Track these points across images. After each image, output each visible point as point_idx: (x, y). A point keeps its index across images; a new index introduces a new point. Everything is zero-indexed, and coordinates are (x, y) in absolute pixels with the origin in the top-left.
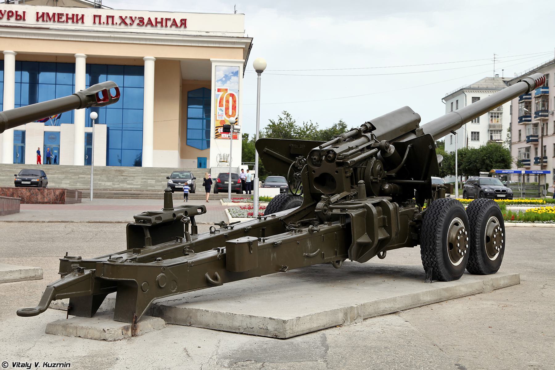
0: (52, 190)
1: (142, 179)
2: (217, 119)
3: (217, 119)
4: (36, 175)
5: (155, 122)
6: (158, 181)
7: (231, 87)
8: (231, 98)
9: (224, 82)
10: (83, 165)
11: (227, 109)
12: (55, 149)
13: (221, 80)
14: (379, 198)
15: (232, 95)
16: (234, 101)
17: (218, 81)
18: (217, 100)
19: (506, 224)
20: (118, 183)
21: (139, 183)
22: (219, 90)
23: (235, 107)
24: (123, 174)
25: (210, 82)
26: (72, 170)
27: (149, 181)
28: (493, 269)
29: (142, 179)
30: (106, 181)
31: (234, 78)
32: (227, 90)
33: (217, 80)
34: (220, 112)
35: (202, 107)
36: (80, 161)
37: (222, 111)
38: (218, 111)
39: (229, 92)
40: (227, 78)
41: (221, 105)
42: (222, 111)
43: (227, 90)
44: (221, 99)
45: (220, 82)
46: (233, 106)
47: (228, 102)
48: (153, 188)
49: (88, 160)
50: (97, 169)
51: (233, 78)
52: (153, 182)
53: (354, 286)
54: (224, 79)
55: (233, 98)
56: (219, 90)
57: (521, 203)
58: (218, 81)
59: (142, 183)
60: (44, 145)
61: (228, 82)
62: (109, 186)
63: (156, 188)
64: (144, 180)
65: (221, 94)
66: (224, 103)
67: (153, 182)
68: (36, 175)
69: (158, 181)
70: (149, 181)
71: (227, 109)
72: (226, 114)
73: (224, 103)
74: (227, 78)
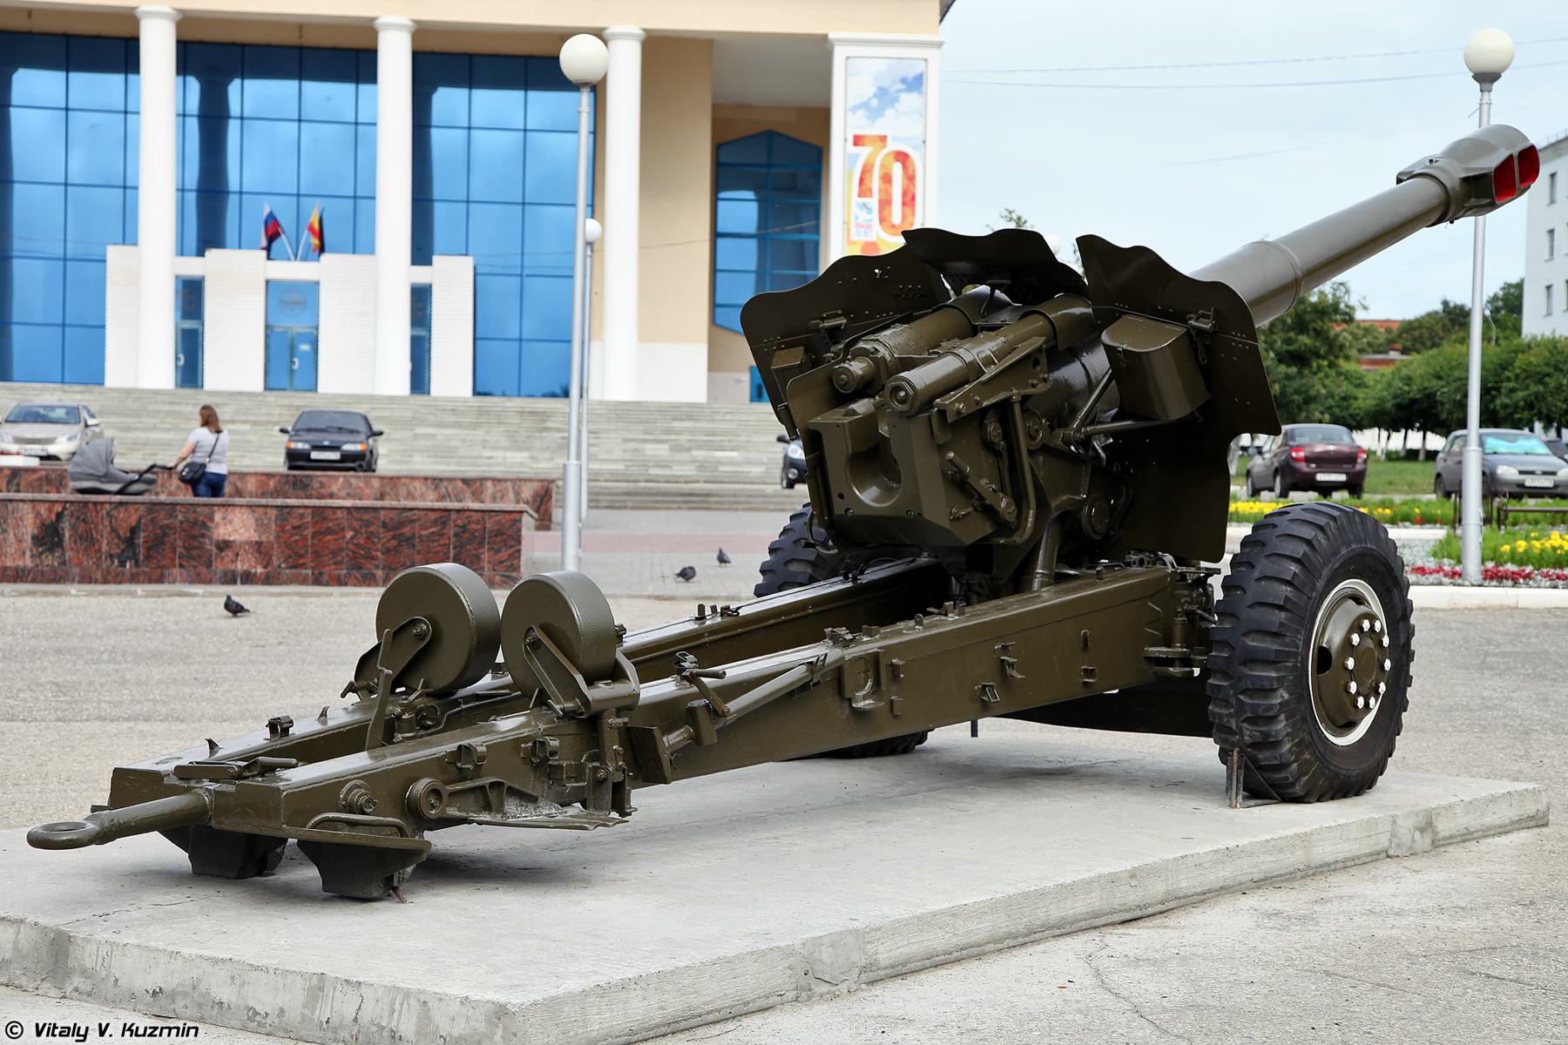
0: (509, 484)
1: (626, 440)
2: (853, 238)
3: (853, 238)
4: (352, 432)
5: (643, 247)
6: (676, 448)
7: (898, 126)
8: (897, 169)
9: (875, 113)
10: (258, 385)
11: (885, 203)
12: (302, 337)
13: (865, 105)
14: (1075, 495)
15: (902, 157)
16: (910, 178)
17: (855, 109)
18: (850, 174)
19: (1419, 595)
20: (547, 455)
21: (618, 454)
22: (858, 141)
23: (913, 198)
24: (549, 424)
25: (822, 116)
26: (138, 399)
27: (651, 450)
28: (1351, 780)
29: (626, 440)
30: (506, 449)
31: (909, 100)
32: (883, 139)
33: (850, 104)
34: (863, 215)
35: (750, 195)
36: (159, 371)
37: (870, 211)
38: (855, 210)
39: (892, 146)
40: (885, 97)
41: (864, 191)
42: (870, 211)
43: (883, 139)
44: (866, 171)
45: (861, 113)
46: (904, 194)
47: (887, 179)
48: (667, 472)
49: (419, 380)
50: (453, 408)
51: (904, 97)
52: (662, 451)
53: (436, 891)
54: (875, 102)
55: (904, 167)
56: (858, 141)
57: (649, 494)
58: (855, 109)
59: (629, 456)
60: (267, 327)
61: (889, 112)
62: (521, 464)
63: (678, 471)
64: (632, 445)
65: (864, 152)
66: (875, 183)
67: (662, 451)
68: (352, 432)
69: (676, 448)
70: (651, 450)
71: (885, 203)
72: (882, 220)
73: (875, 183)
74: (885, 97)
